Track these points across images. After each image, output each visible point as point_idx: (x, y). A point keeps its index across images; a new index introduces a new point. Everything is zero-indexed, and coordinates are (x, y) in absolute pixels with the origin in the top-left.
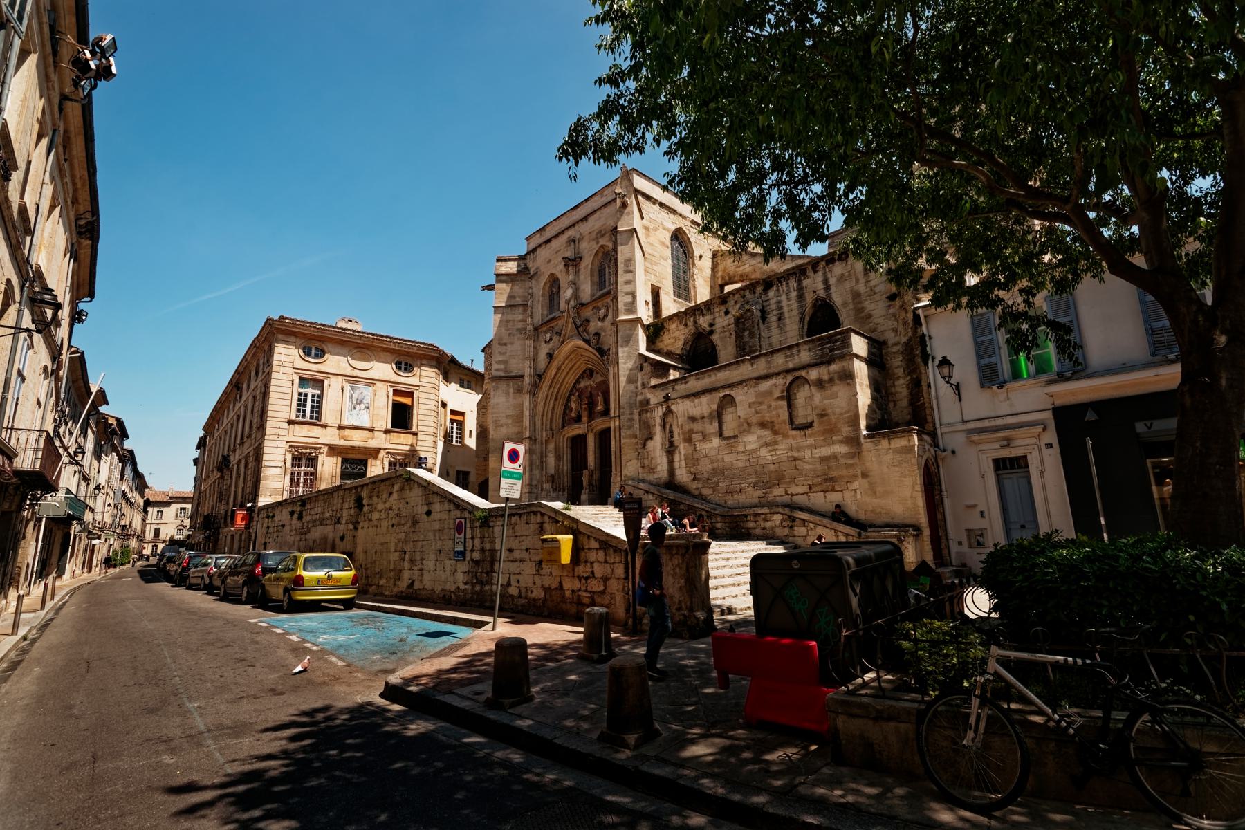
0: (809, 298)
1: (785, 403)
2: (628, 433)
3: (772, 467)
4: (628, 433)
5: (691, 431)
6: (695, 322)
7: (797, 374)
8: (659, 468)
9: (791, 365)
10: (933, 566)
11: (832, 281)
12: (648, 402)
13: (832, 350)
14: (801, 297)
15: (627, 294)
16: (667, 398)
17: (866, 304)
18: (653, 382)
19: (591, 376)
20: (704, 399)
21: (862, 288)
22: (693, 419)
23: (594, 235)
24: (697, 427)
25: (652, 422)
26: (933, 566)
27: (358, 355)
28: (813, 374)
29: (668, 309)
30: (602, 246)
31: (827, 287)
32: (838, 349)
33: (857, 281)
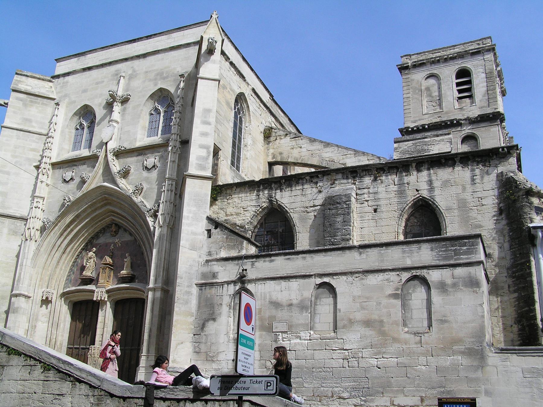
0: (411, 196)
1: (398, 302)
2: (183, 309)
3: (375, 372)
4: (183, 309)
5: (273, 318)
6: (270, 196)
7: (415, 272)
8: (222, 357)
9: (409, 263)
10: (108, 303)
11: (436, 184)
12: (214, 276)
13: (457, 253)
14: (401, 193)
15: (202, 147)
16: (242, 279)
17: (473, 214)
18: (224, 254)
19: (116, 233)
20: (294, 284)
21: (468, 196)
22: (276, 305)
23: (152, 76)
24: (282, 314)
25: (217, 300)
26: (108, 303)
27: (510, 321)
28: (434, 276)
29: (225, 175)
30: (161, 90)
31: (431, 189)
32: (465, 253)
33: (464, 189)
